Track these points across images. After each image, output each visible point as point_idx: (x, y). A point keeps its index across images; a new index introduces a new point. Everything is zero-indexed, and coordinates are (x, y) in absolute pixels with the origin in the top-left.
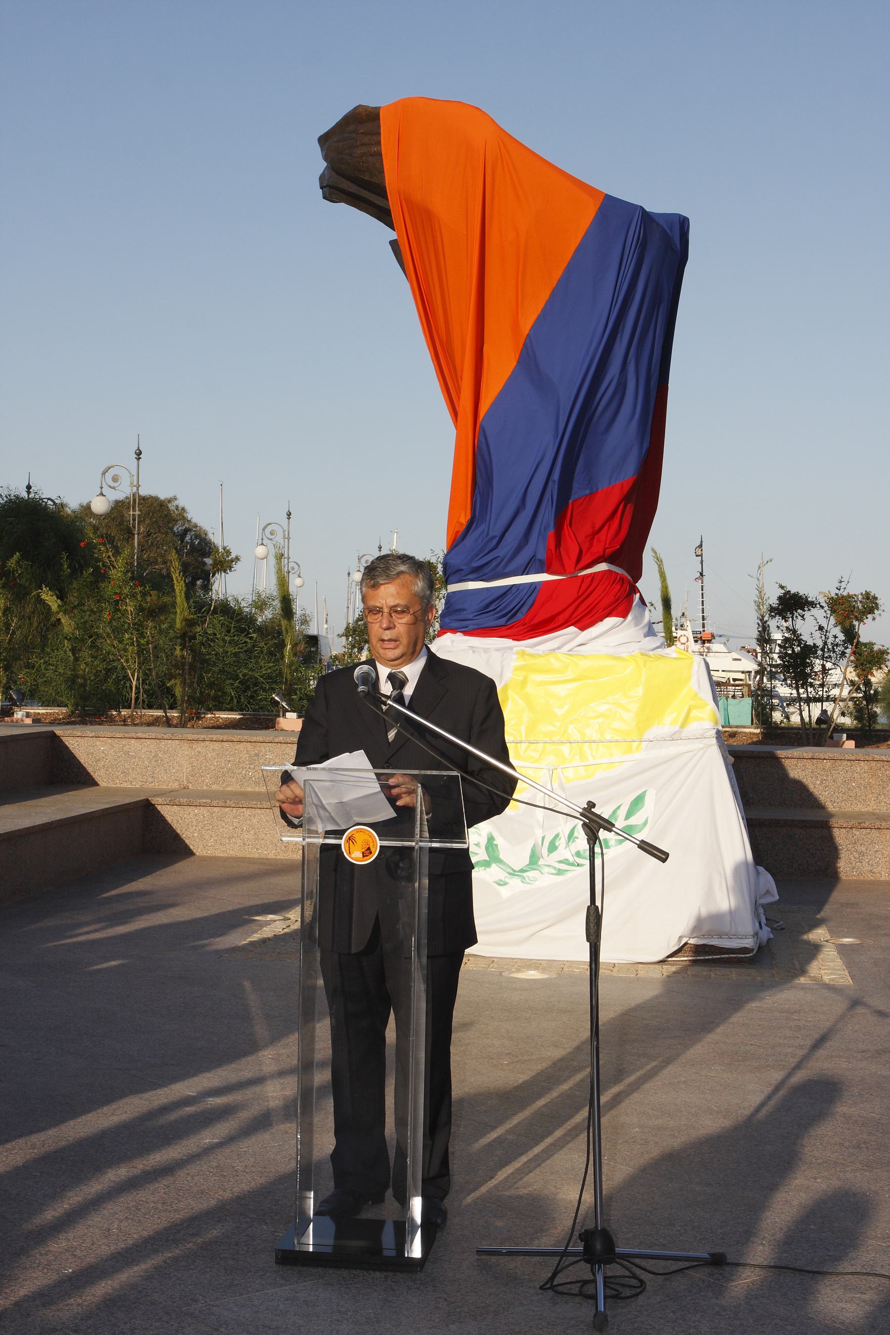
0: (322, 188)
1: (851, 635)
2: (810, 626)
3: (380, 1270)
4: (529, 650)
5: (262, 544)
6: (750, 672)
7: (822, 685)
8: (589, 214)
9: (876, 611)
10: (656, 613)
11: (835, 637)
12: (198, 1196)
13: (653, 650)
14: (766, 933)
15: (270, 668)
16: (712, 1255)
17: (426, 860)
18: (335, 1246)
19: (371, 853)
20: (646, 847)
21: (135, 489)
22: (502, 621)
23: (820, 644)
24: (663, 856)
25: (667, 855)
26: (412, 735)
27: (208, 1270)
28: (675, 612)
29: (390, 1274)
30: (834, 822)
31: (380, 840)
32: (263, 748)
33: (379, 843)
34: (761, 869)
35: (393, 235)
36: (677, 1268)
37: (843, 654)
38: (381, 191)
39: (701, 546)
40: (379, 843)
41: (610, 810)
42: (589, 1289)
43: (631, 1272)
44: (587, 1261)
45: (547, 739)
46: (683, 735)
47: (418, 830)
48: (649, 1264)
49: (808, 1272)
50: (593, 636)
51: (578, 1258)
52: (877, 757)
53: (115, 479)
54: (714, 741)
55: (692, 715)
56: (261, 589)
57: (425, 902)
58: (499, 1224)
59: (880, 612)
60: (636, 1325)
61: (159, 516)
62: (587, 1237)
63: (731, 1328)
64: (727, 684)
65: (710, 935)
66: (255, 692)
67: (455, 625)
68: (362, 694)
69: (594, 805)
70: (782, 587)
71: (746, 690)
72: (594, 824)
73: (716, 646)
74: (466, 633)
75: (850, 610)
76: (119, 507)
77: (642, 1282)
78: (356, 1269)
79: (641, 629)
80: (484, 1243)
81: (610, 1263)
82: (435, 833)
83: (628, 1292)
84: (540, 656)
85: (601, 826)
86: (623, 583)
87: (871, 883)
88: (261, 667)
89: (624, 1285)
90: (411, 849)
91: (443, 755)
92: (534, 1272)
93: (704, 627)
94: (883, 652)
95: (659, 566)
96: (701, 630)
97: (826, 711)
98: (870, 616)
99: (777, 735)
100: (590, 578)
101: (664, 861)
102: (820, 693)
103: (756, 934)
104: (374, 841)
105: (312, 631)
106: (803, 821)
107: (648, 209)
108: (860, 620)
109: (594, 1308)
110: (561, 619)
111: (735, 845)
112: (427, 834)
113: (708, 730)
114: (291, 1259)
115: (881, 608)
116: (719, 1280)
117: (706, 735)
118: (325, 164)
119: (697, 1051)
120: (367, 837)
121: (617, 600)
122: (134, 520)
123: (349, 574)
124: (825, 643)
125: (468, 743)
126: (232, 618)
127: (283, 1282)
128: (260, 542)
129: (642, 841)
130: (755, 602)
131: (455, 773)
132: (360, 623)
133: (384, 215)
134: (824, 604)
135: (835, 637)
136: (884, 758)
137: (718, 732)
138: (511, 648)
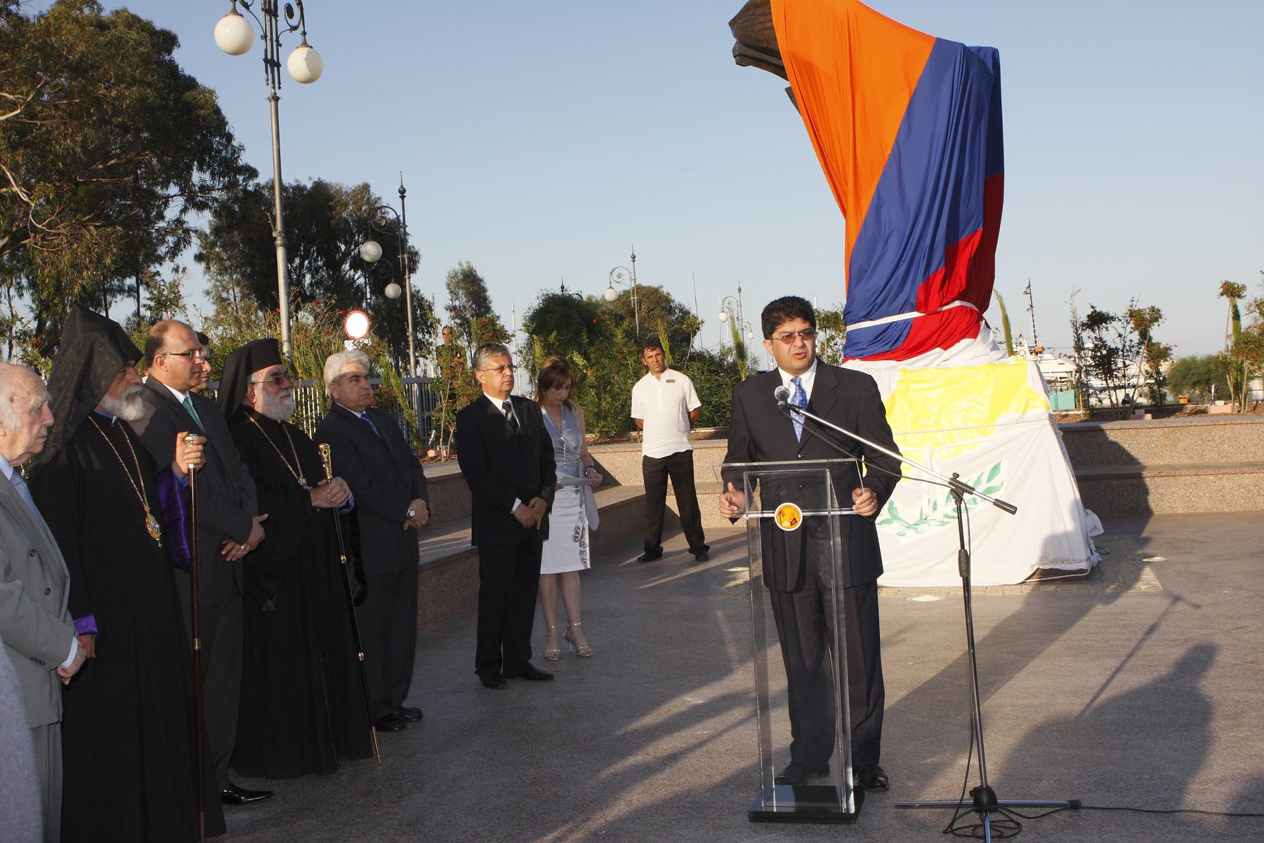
1: (1144, 335)
2: (1110, 335)
7: (1124, 376)
8: (926, 52)
14: (1096, 557)
16: (1071, 802)
17: (837, 525)
20: (999, 504)
22: (887, 348)
23: (1120, 347)
24: (1012, 510)
28: (1014, 334)
30: (1145, 473)
33: (802, 514)
35: (787, 84)
37: (1138, 353)
38: (777, 54)
40: (802, 514)
41: (972, 474)
42: (980, 832)
44: (977, 811)
47: (829, 503)
48: (1019, 810)
53: (619, 276)
54: (1048, 422)
57: (839, 555)
58: (911, 784)
61: (656, 300)
62: (976, 793)
64: (1055, 381)
65: (1055, 561)
73: (1046, 355)
74: (862, 359)
75: (1143, 321)
76: (624, 298)
77: (1018, 824)
83: (1009, 833)
87: (1170, 515)
94: (1168, 349)
103: (1089, 559)
110: (930, 342)
111: (1067, 490)
118: (735, 40)
119: (1054, 647)
125: (857, 434)
133: (780, 71)
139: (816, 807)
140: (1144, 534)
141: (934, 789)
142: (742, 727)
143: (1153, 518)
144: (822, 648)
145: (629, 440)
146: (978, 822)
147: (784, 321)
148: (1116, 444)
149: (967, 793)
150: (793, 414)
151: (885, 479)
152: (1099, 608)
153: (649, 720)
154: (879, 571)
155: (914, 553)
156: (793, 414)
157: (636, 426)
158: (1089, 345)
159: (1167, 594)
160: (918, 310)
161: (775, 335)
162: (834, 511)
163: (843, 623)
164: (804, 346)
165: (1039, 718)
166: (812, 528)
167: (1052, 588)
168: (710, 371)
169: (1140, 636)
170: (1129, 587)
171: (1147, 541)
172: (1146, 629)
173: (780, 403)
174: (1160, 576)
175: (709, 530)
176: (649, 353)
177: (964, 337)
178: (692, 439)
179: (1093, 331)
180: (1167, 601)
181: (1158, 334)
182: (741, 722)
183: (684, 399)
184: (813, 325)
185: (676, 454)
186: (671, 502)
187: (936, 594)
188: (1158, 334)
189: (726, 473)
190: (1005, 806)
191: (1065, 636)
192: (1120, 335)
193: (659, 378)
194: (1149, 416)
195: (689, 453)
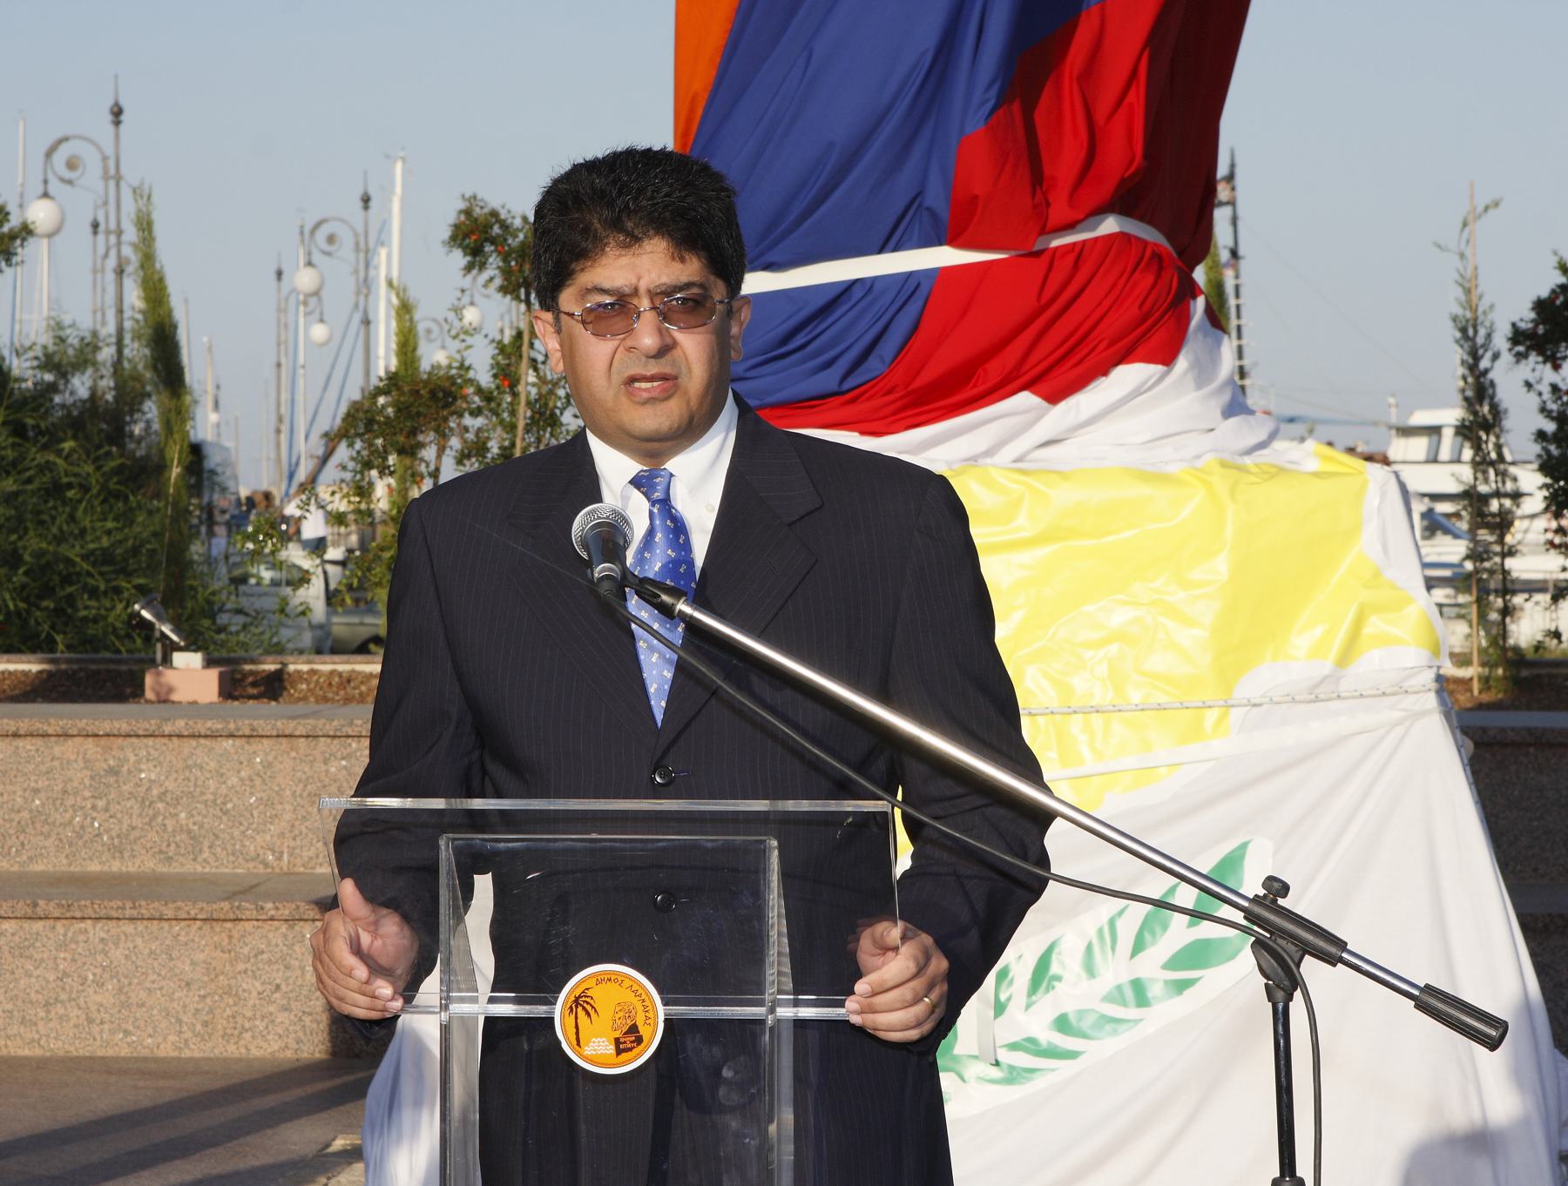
5: (46, 195)
13: (1250, 451)
15: (109, 533)
19: (639, 1040)
22: (828, 380)
31: (665, 1004)
32: (130, 752)
46: (1345, 686)
50: (1084, 416)
54: (1431, 701)
55: (1367, 630)
66: (70, 599)
68: (606, 585)
69: (1284, 889)
72: (1286, 944)
82: (803, 983)
85: (1308, 949)
86: (1161, 268)
88: (83, 532)
90: (760, 1022)
100: (1071, 258)
110: (995, 369)
117: (1406, 685)
123: (279, 274)
125: (884, 696)
128: (40, 190)
129: (1429, 989)
130: (1455, 319)
132: (381, 400)
150: (635, 605)
151: (986, 878)
156: (635, 605)
161: (568, 299)
164: (666, 349)
166: (686, 1070)
177: (1125, 357)
189: (356, 840)
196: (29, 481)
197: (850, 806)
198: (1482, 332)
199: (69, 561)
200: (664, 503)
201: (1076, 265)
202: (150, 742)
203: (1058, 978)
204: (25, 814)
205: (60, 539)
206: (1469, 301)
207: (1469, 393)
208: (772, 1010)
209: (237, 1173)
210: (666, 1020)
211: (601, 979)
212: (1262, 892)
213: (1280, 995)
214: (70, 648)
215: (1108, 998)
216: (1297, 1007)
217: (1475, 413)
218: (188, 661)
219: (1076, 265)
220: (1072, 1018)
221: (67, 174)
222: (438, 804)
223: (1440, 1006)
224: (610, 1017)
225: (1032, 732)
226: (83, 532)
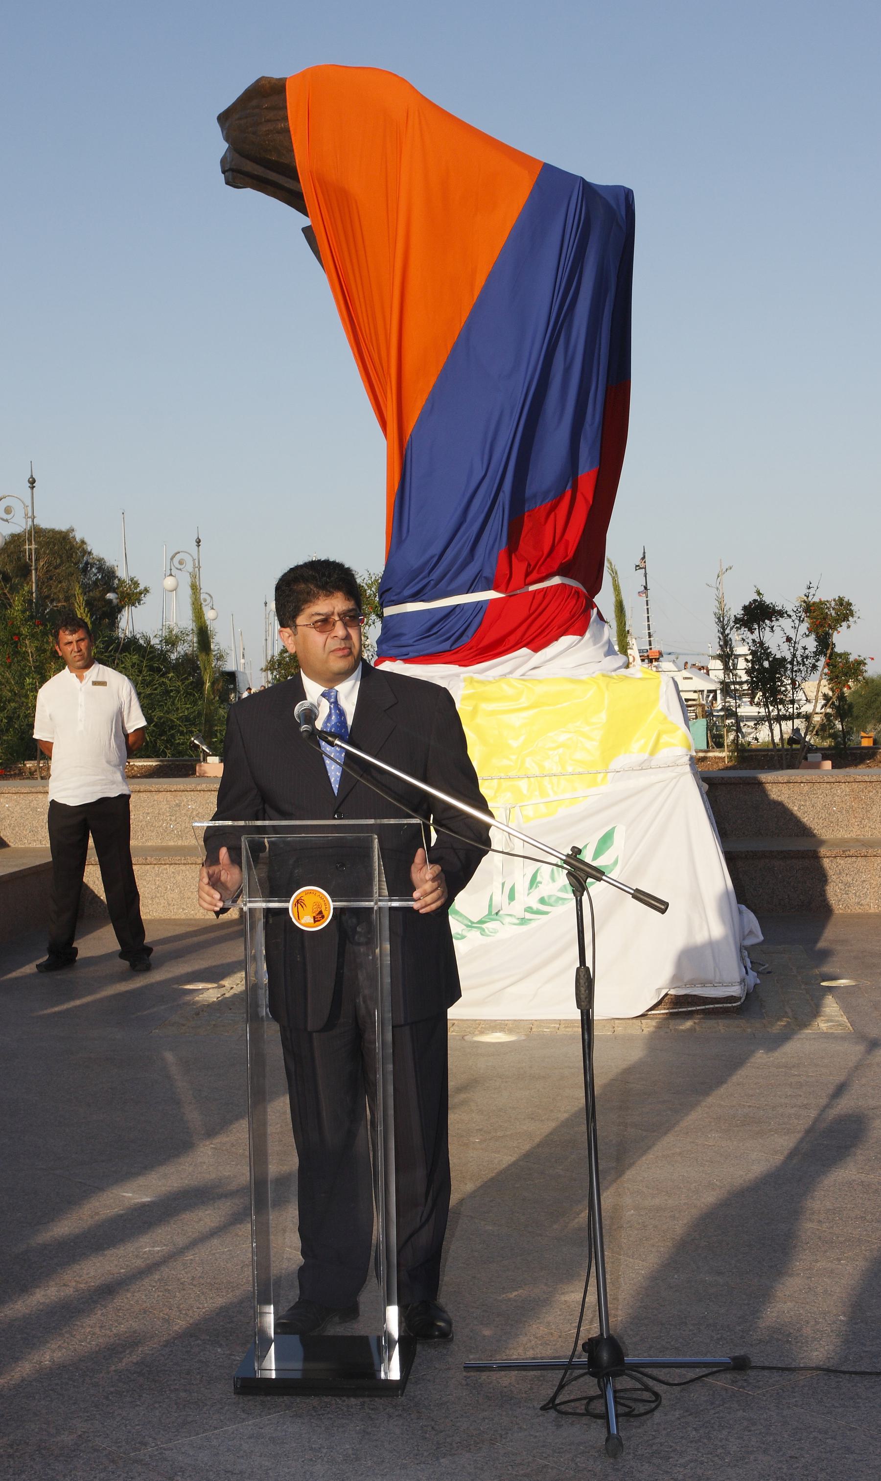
0: (223, 172)
1: (824, 644)
2: (775, 639)
3: (355, 1396)
4: (477, 677)
5: (171, 575)
6: (702, 691)
8: (513, 200)
9: (850, 618)
10: (610, 632)
11: (805, 648)
12: (141, 1317)
13: (615, 670)
14: (753, 978)
15: (188, 709)
16: (734, 1359)
17: (386, 922)
18: (304, 1370)
19: (323, 917)
20: (640, 896)
21: (30, 520)
22: (446, 646)
23: (789, 657)
24: (661, 906)
25: (667, 905)
26: (361, 776)
27: (157, 1405)
29: (367, 1400)
30: (823, 851)
31: (333, 901)
32: (185, 797)
33: (332, 905)
34: (743, 907)
35: (306, 222)
36: (694, 1376)
37: (814, 667)
38: (292, 173)
39: (644, 558)
42: (597, 1407)
43: (642, 1383)
44: (593, 1375)
45: (502, 775)
47: (376, 889)
48: (661, 1373)
49: (844, 1372)
50: (548, 657)
51: (582, 1371)
52: (859, 778)
54: (688, 768)
55: (661, 741)
56: (172, 624)
57: (387, 971)
58: (487, 1332)
59: (855, 619)
60: (655, 1448)
61: (62, 549)
62: (592, 1346)
63: (764, 1446)
65: (692, 983)
67: (393, 652)
68: (305, 734)
70: (759, 593)
71: (699, 710)
75: (825, 618)
77: (656, 1394)
78: (327, 1396)
79: (600, 648)
80: (471, 1357)
81: (621, 1375)
82: (393, 893)
83: (641, 1408)
84: (490, 682)
87: (859, 916)
88: (178, 709)
89: (636, 1400)
91: (400, 798)
92: (531, 1389)
93: (650, 645)
94: (860, 663)
95: (613, 578)
96: (648, 647)
97: (798, 730)
98: (844, 624)
99: (747, 756)
101: (663, 911)
102: (791, 710)
103: (743, 981)
104: (326, 904)
105: (230, 666)
106: (782, 852)
107: (588, 179)
108: (835, 629)
109: (605, 1430)
110: (512, 639)
111: (715, 877)
112: (386, 892)
113: (681, 756)
114: (252, 1387)
115: (856, 615)
116: (744, 1388)
117: (677, 762)
118: (225, 146)
119: (694, 1117)
120: (319, 900)
121: (573, 616)
122: (30, 554)
123: (266, 604)
124: (794, 656)
126: (144, 657)
127: (244, 1416)
129: (637, 890)
131: (416, 821)
133: (296, 200)
134: (791, 613)
135: (805, 648)
136: (866, 778)
137: (691, 758)
138: (457, 675)
139: (335, 1370)
140: (821, 945)
141: (523, 1339)
142: (215, 1241)
143: (833, 920)
144: (354, 1114)
145: (20, 774)
146: (595, 1391)
147: (316, 597)
148: (780, 805)
149: (580, 1348)
150: (325, 747)
151: (463, 853)
152: (760, 1057)
153: (65, 1227)
154: (453, 992)
155: (511, 968)
157: (40, 752)
158: (742, 650)
159: (860, 1036)
160: (496, 588)
161: (301, 620)
162: (381, 901)
163: (390, 1078)
164: (348, 637)
165: (679, 1227)
166: (348, 926)
167: (689, 1024)
168: (151, 669)
169: (824, 1101)
170: (804, 1025)
171: (825, 955)
172: (831, 1090)
173: (304, 727)
174: (847, 1009)
175: (150, 921)
176: (67, 637)
178: (130, 776)
179: (751, 631)
180: (861, 1048)
181: (843, 640)
182: (214, 1233)
183: (119, 715)
184: (358, 603)
185: (103, 801)
186: (93, 877)
187: (510, 1031)
188: (843, 640)
190: (636, 1367)
191: (710, 1100)
192: (789, 639)
193: (81, 678)
194: (827, 765)
195: (124, 799)
196: (156, 689)
197: (405, 821)
198: (726, 619)
199: (172, 721)
200: (336, 703)
201: (544, 597)
202: (192, 793)
203: (540, 883)
204: (144, 823)
205: (168, 712)
206: (721, 607)
207: (722, 643)
208: (376, 904)
209: (222, 965)
210: (334, 909)
211: (308, 893)
212: (570, 853)
213: (578, 894)
214: (173, 755)
215: (561, 890)
216: (585, 898)
217: (724, 651)
218: (214, 760)
219: (544, 597)
220: (546, 898)
221: (179, 567)
222: (242, 823)
223: (642, 897)
224: (311, 908)
225: (484, 789)
226: (178, 709)
